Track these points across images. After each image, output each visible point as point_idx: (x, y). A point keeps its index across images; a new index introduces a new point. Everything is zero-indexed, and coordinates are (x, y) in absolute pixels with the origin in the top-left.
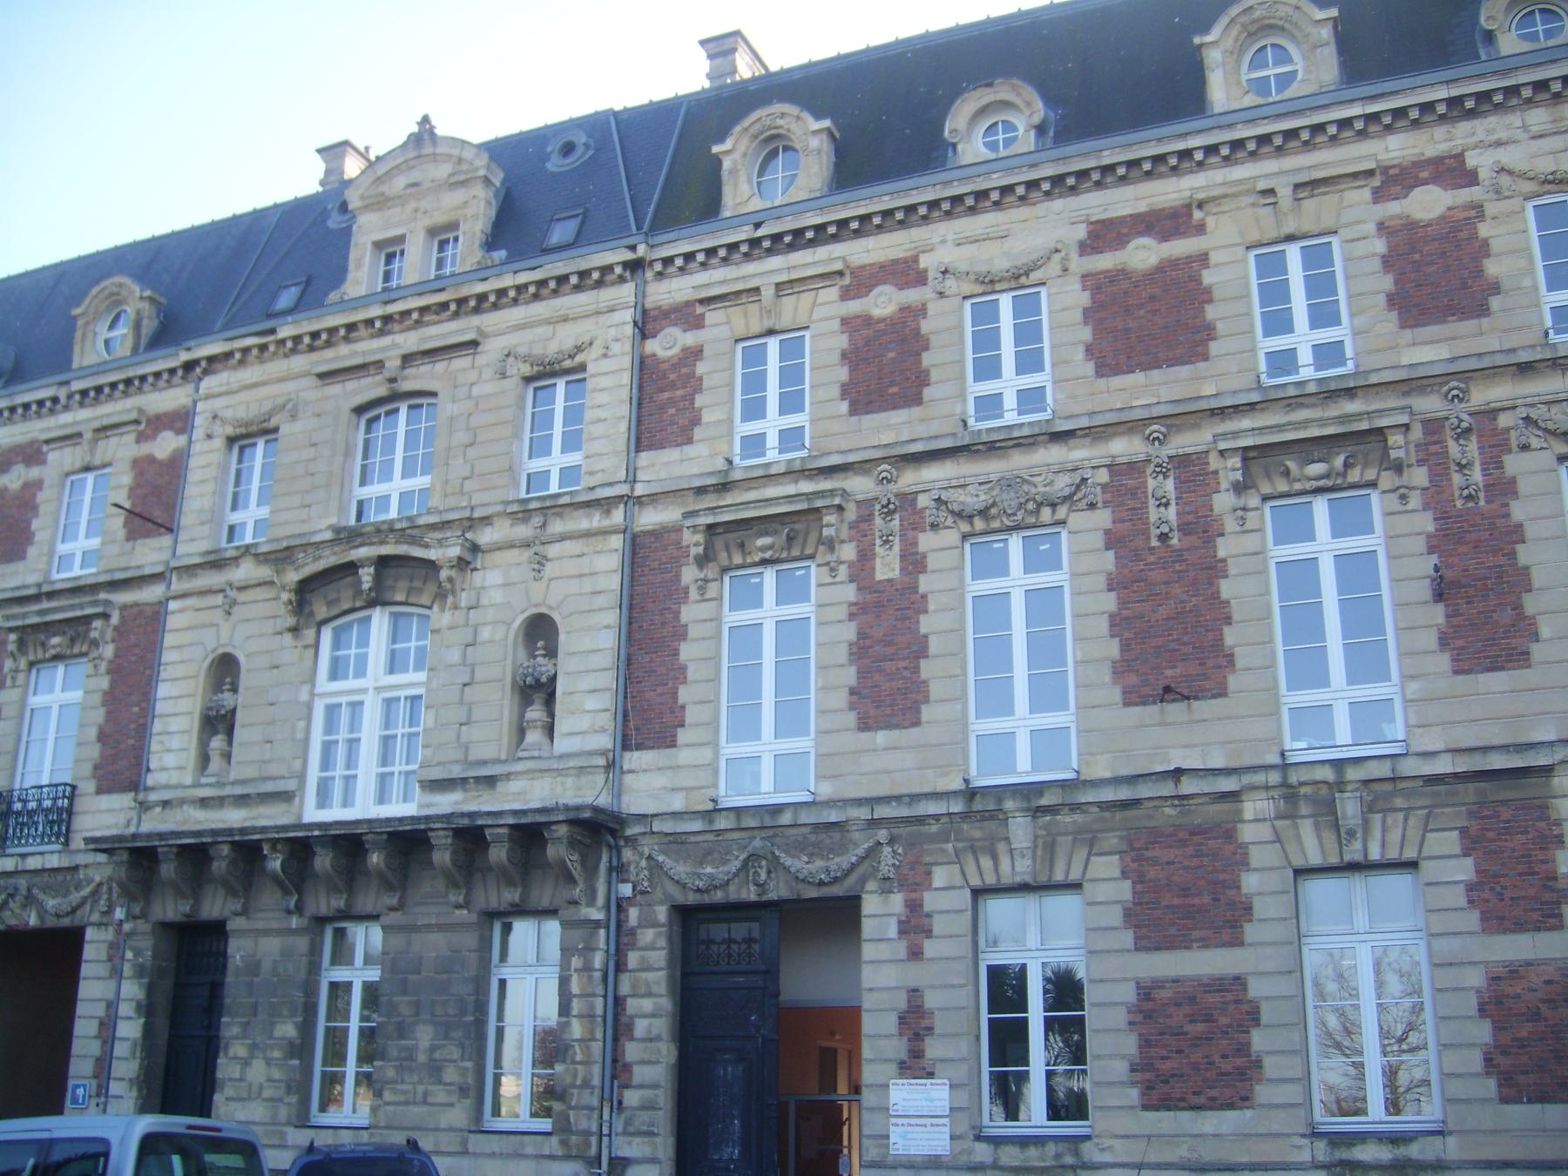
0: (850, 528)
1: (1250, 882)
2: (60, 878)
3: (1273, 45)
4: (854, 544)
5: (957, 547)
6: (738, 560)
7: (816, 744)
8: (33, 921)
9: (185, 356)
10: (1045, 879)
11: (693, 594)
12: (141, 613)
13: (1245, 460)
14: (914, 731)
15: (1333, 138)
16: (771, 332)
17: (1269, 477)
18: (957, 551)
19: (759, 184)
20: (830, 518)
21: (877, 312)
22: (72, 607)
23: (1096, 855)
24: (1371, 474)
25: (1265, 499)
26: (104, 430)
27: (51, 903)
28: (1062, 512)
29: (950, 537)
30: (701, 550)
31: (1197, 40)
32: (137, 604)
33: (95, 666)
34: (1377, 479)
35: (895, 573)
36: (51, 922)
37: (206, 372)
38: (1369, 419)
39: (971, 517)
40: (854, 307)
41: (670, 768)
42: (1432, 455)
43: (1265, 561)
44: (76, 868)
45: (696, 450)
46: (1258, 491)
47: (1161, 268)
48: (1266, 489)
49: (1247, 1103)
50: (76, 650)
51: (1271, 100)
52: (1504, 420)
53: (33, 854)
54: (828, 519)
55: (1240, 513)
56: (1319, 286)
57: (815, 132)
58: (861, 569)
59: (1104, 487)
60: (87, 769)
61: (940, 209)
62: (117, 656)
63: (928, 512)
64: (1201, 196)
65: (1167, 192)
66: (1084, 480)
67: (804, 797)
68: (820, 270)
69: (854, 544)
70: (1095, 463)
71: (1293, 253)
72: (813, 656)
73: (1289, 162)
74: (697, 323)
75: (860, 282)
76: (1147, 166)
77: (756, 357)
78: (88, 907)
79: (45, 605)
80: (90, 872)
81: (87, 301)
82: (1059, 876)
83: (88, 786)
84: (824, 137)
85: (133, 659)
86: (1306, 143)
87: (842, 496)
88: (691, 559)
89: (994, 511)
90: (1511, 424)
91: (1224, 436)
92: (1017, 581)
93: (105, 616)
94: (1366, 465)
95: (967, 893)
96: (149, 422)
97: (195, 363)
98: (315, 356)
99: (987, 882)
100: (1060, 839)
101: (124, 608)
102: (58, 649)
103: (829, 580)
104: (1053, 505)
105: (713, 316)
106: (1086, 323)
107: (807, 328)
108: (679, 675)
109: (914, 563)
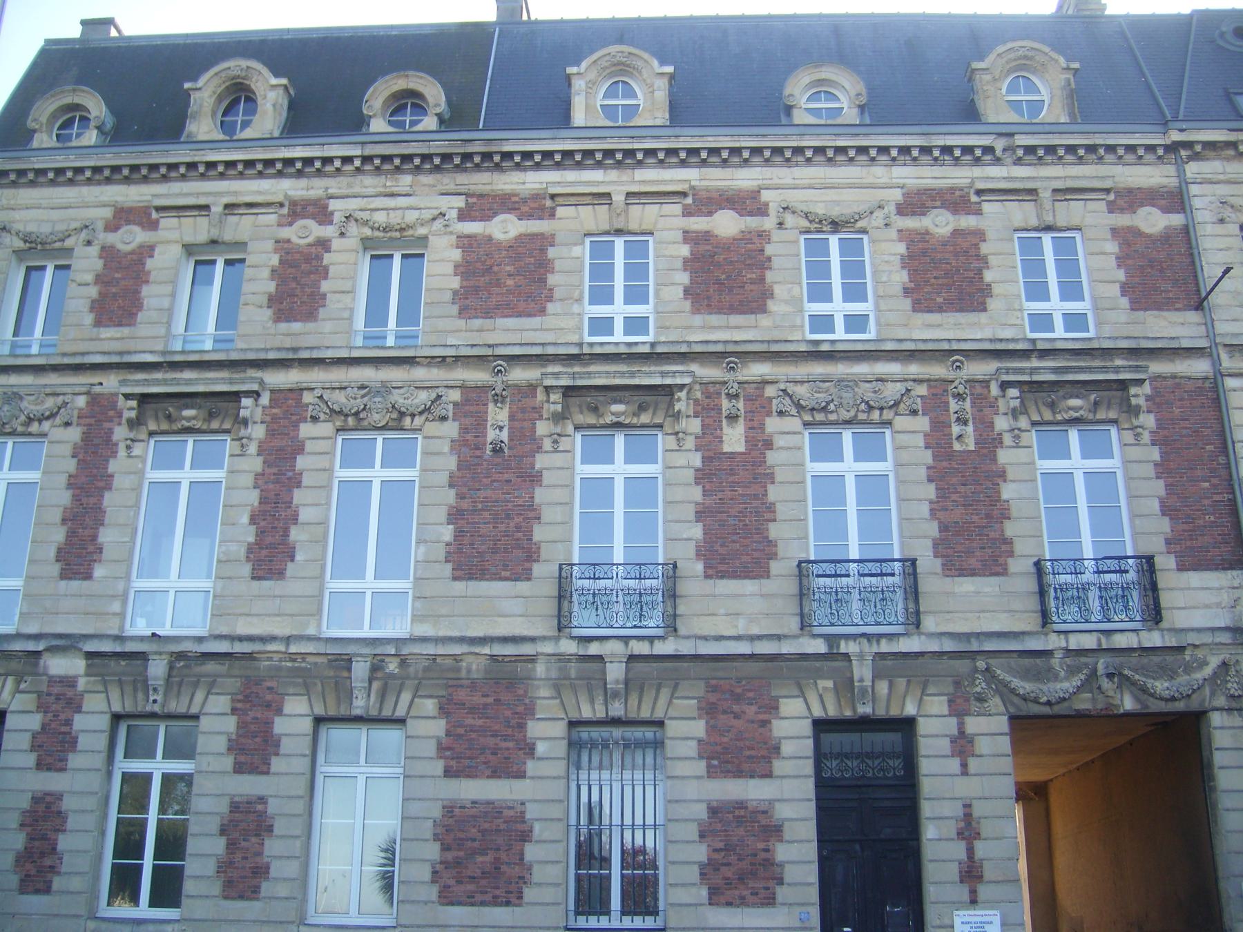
1: (534, 729)
2: (1156, 659)
4: (264, 426)
5: (331, 438)
6: (1048, 416)
8: (1129, 704)
9: (1176, 136)
11: (1008, 439)
12: (1178, 386)
13: (565, 395)
14: (86, 583)
15: (619, 163)
16: (619, 232)
17: (157, 418)
18: (330, 442)
20: (246, 402)
21: (498, 235)
22: (1090, 370)
25: (1034, 424)
26: (1064, 193)
28: (418, 421)
29: (326, 428)
30: (133, 414)
31: (187, 85)
32: (1174, 377)
34: (422, 426)
35: (740, 447)
36: (1156, 706)
37: (1196, 157)
38: (574, 378)
40: (1123, 220)
41: (269, 596)
42: (708, 410)
43: (331, 478)
44: (1180, 649)
46: (147, 427)
47: (520, 238)
48: (152, 426)
50: (1101, 415)
51: (617, 125)
52: (770, 391)
55: (129, 442)
56: (636, 271)
57: (274, 87)
58: (708, 442)
59: (455, 404)
60: (691, 550)
63: (311, 407)
64: (552, 190)
65: (744, 178)
69: (264, 426)
70: (77, 390)
71: (619, 243)
72: (810, 509)
73: (626, 175)
74: (153, 226)
75: (706, 203)
77: (602, 251)
78: (1207, 691)
79: (1035, 363)
80: (1200, 654)
82: (387, 713)
83: (928, 563)
84: (281, 91)
85: (1184, 432)
86: (457, 166)
87: (260, 384)
88: (124, 421)
89: (832, 407)
91: (1008, 371)
92: (849, 466)
93: (257, 394)
94: (1109, 407)
95: (107, 717)
97: (1188, 145)
98: (303, 182)
99: (370, 713)
101: (1158, 377)
102: (1082, 412)
103: (1133, 441)
104: (413, 416)
105: (168, 223)
107: (651, 233)
108: (701, 514)
109: (760, 443)
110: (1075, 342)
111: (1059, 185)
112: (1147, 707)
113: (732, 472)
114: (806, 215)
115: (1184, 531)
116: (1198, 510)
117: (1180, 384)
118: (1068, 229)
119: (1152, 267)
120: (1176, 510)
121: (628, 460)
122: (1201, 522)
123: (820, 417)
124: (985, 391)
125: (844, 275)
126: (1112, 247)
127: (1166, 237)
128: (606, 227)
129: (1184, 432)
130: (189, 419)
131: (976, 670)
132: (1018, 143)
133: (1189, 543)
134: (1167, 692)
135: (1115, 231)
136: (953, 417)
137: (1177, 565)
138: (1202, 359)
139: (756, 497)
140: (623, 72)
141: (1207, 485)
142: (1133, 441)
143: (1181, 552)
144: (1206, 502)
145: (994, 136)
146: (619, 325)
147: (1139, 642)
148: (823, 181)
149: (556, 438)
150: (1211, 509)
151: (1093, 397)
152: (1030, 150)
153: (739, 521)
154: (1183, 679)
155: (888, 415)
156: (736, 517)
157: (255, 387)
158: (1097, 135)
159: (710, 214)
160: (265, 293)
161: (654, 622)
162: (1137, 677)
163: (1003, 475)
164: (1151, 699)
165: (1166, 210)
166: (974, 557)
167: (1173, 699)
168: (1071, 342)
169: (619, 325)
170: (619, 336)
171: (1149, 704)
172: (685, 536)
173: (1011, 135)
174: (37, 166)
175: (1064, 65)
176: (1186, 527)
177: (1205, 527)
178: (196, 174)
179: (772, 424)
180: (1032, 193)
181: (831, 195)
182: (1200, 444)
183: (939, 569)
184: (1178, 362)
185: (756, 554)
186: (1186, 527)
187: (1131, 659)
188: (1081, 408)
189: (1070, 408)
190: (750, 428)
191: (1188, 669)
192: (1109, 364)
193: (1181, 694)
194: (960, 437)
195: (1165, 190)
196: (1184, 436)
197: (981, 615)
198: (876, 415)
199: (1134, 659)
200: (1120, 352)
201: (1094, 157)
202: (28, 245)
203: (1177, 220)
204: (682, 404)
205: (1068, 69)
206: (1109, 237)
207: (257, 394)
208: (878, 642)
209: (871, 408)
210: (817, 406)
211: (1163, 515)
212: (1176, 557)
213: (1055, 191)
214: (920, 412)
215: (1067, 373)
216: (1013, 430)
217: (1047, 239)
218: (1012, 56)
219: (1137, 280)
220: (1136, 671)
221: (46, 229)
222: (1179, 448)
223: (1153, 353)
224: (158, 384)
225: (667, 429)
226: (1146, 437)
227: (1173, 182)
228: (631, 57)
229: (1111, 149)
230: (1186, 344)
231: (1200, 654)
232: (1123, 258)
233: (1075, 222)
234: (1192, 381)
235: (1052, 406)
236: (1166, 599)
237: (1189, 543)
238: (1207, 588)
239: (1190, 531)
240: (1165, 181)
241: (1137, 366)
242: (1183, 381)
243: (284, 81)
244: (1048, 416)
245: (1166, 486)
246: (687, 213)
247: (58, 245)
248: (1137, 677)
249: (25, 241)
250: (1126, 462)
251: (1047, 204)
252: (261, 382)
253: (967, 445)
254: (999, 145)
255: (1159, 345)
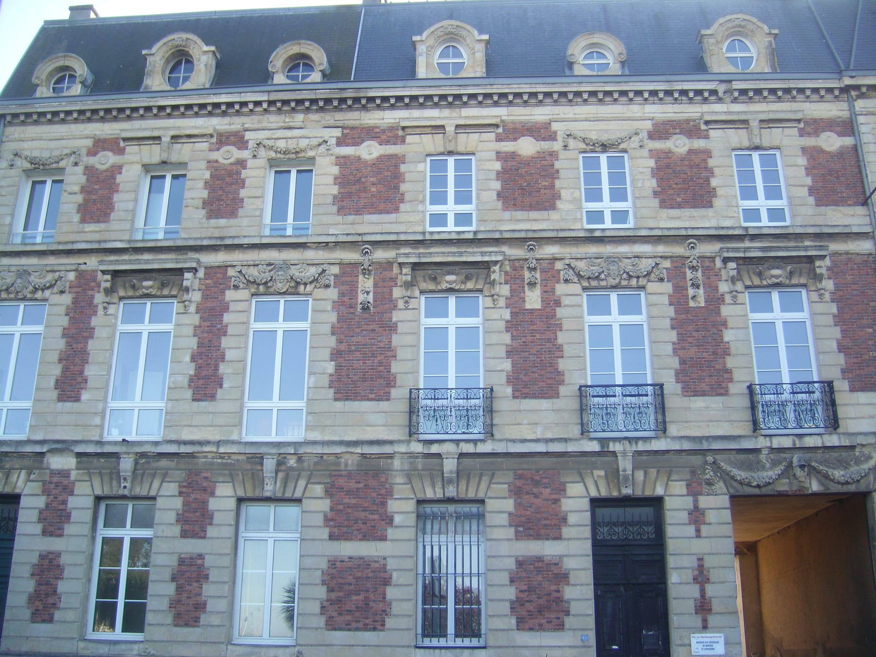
0: (827, 270)
2: (835, 455)
3: (453, 46)
5: (247, 301)
6: (757, 281)
7: (307, 404)
9: (847, 81)
10: (474, 496)
11: (728, 299)
13: (413, 269)
14: (76, 404)
16: (450, 153)
17: (125, 288)
19: (169, 78)
20: (187, 275)
21: (365, 156)
22: (787, 249)
23: (312, 483)
24: (803, 281)
25: (747, 287)
26: (768, 123)
27: (838, 474)
28: (309, 288)
29: (244, 294)
30: (108, 285)
31: (144, 52)
32: (847, 253)
33: (185, 307)
35: (538, 306)
36: (835, 488)
37: (862, 96)
39: (259, 285)
40: (810, 142)
43: (247, 329)
44: (852, 448)
45: (554, 215)
47: (381, 158)
48: (122, 293)
49: (197, 624)
51: (449, 77)
52: (559, 265)
53: (810, 435)
54: (818, 263)
55: (105, 305)
56: (463, 181)
58: (515, 301)
59: (336, 276)
61: (346, 103)
62: (205, 297)
64: (403, 124)
65: (539, 114)
66: (324, 271)
67: (22, 437)
68: (433, 123)
71: (451, 161)
74: (121, 151)
75: (513, 132)
76: (168, 110)
79: (747, 244)
80: (866, 451)
81: (716, 26)
82: (288, 495)
83: (672, 387)
84: (211, 55)
85: (854, 293)
88: (102, 290)
89: (603, 276)
90: (234, 274)
91: (728, 250)
92: (615, 318)
93: (195, 270)
94: (800, 275)
95: (92, 499)
96: (807, 123)
97: (857, 87)
98: (227, 120)
100: (302, 473)
101: (835, 254)
102: (781, 279)
103: (818, 299)
104: (305, 284)
106: (498, 180)
108: (510, 353)
109: (552, 302)
110: (776, 229)
111: (764, 117)
112: (829, 489)
113: (532, 323)
114: (584, 140)
115: (854, 363)
116: (864, 348)
117: (851, 258)
118: (771, 149)
119: (831, 175)
120: (848, 348)
121: (458, 315)
122: (867, 357)
123: (594, 283)
124: (712, 264)
125: (764, 181)
126: (802, 161)
127: (841, 154)
128: (442, 150)
129: (854, 293)
130: (147, 288)
131: (706, 462)
132: (735, 87)
133: (858, 372)
134: (843, 478)
135: (804, 149)
136: (689, 283)
137: (850, 388)
138: (867, 241)
139: (549, 340)
140: (452, 39)
141: (871, 330)
142: (818, 299)
143: (852, 378)
144: (870, 343)
145: (718, 82)
146: (451, 219)
147: (823, 443)
148: (596, 115)
149: (407, 300)
150: (874, 348)
151: (789, 268)
152: (744, 92)
153: (537, 358)
154: (854, 469)
155: (642, 282)
156: (536, 355)
157: (194, 265)
158: (791, 81)
159: (515, 139)
160: (201, 198)
161: (477, 429)
162: (821, 467)
163: (724, 324)
164: (831, 483)
165: (841, 134)
166: (704, 382)
167: (847, 483)
168: (773, 229)
169: (451, 219)
170: (451, 227)
171: (830, 487)
172: (499, 369)
173: (730, 81)
174: (39, 110)
175: (768, 32)
176: (855, 360)
177: (870, 360)
178: (151, 115)
179: (561, 289)
180: (440, 129)
181: (602, 125)
182: (866, 301)
183: (679, 391)
184: (850, 243)
185: (549, 382)
186: (855, 360)
187: (817, 454)
188: (780, 276)
189: (773, 276)
190: (544, 292)
191: (858, 462)
192: (800, 244)
193: (853, 479)
194: (694, 297)
195: (840, 120)
196: (854, 296)
197: (710, 424)
198: (634, 282)
199: (819, 455)
200: (808, 236)
201: (789, 97)
202: (33, 166)
203: (848, 141)
204: (496, 275)
205: (770, 34)
206: (800, 153)
207: (822, 257)
208: (636, 443)
209: (630, 277)
210: (592, 276)
211: (840, 352)
212: (849, 382)
213: (761, 121)
214: (666, 280)
215: (770, 251)
216: (732, 292)
217: (756, 156)
218: (730, 25)
219: (820, 184)
220: (820, 463)
221: (46, 154)
222: (852, 304)
223: (832, 236)
224: (125, 263)
225: (486, 293)
226: (827, 296)
227: (846, 114)
228: (459, 28)
229: (801, 91)
230: (855, 230)
231: (866, 451)
232: (810, 168)
233: (776, 143)
234: (860, 256)
235: (760, 275)
236: (841, 412)
237: (858, 372)
238: (871, 404)
239: (858, 363)
240: (840, 114)
241: (821, 246)
242: (853, 257)
243: (213, 48)
244: (757, 281)
245: (842, 331)
246: (499, 139)
247: (54, 166)
248: (821, 467)
249: (32, 163)
250: (813, 314)
251: (756, 131)
252: (198, 262)
253: (699, 303)
254: (721, 88)
255: (836, 230)
